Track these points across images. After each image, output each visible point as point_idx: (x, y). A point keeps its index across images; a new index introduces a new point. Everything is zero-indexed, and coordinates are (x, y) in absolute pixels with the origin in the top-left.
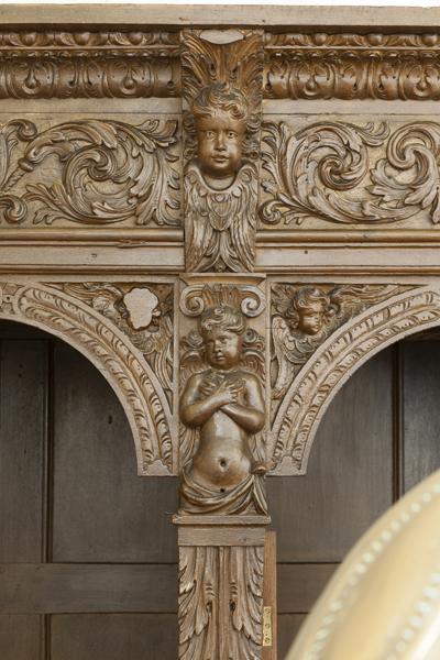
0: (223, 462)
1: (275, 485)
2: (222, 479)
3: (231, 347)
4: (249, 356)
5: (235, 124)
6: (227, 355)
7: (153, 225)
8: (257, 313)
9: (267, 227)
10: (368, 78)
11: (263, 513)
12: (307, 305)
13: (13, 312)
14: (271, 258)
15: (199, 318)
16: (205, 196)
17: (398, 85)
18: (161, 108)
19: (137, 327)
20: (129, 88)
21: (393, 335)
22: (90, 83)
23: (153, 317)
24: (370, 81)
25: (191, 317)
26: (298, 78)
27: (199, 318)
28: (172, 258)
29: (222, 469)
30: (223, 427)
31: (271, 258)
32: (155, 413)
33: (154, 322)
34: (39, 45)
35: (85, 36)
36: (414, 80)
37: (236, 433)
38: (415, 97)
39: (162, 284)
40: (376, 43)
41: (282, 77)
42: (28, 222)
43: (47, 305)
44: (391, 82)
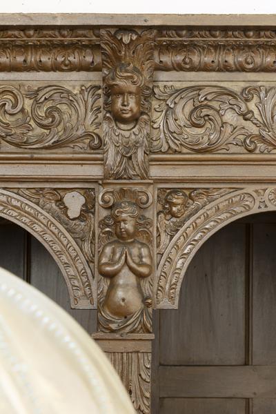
0: (123, 300)
1: (161, 314)
2: (124, 314)
3: (129, 226)
4: (142, 233)
5: (133, 88)
6: (127, 231)
7: (171, 152)
8: (145, 206)
9: (92, 151)
10: (32, 58)
11: (150, 333)
12: (172, 199)
13: (266, 206)
14: (155, 172)
15: (110, 208)
16: (118, 135)
17: (200, 62)
18: (94, 78)
19: (71, 218)
20: (66, 66)
21: (230, 217)
22: (40, 61)
23: (81, 211)
24: (220, 60)
25: (106, 208)
26: (56, 59)
27: (110, 208)
28: (95, 171)
29: (122, 304)
30: (126, 278)
31: (155, 172)
32: (80, 270)
33: (82, 217)
34: (37, 37)
35: (31, 32)
36: (60, 59)
37: (132, 279)
38: (62, 70)
39: (88, 188)
40: (29, 36)
41: (49, 59)
42: (257, 151)
43: (15, 207)
44: (230, 59)
